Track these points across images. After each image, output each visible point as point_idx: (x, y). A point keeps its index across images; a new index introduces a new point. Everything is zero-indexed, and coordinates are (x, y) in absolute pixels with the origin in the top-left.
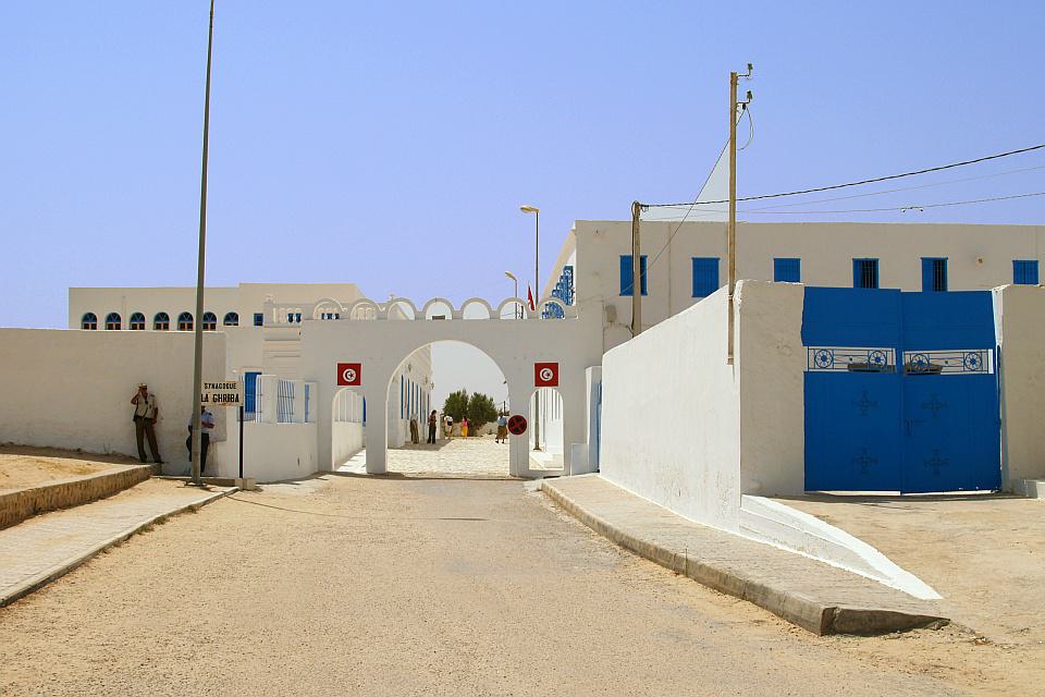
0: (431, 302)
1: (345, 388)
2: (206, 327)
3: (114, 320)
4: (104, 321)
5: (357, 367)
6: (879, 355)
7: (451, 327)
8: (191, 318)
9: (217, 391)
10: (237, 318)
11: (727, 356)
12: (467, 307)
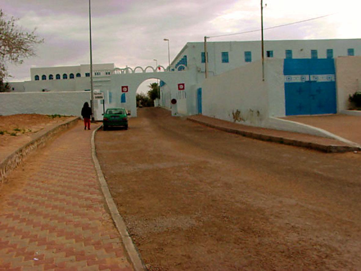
0: (151, 67)
3: (72, 76)
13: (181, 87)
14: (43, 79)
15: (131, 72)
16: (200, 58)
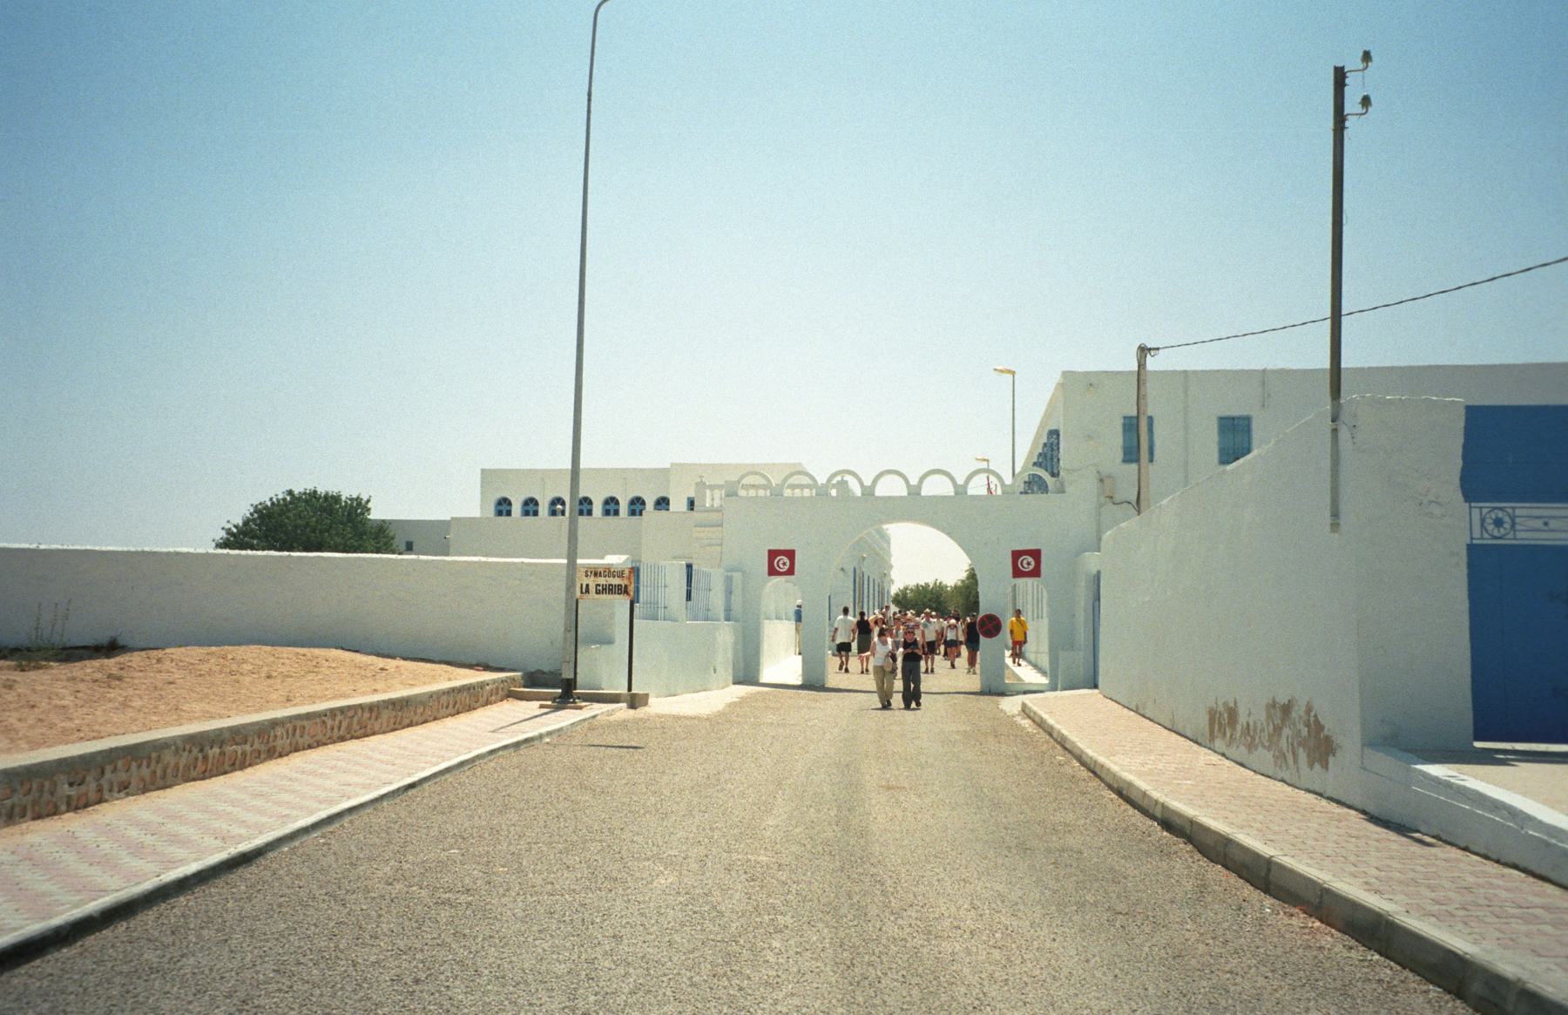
0: (889, 472)
1: (776, 579)
2: (581, 513)
3: (637, 505)
4: (601, 507)
5: (791, 554)
6: (1500, 514)
7: (915, 507)
8: (563, 503)
9: (602, 581)
10: (668, 504)
11: (1328, 519)
12: (897, 477)
13: (1027, 563)
14: (607, 513)
15: (858, 492)
16: (1115, 440)
